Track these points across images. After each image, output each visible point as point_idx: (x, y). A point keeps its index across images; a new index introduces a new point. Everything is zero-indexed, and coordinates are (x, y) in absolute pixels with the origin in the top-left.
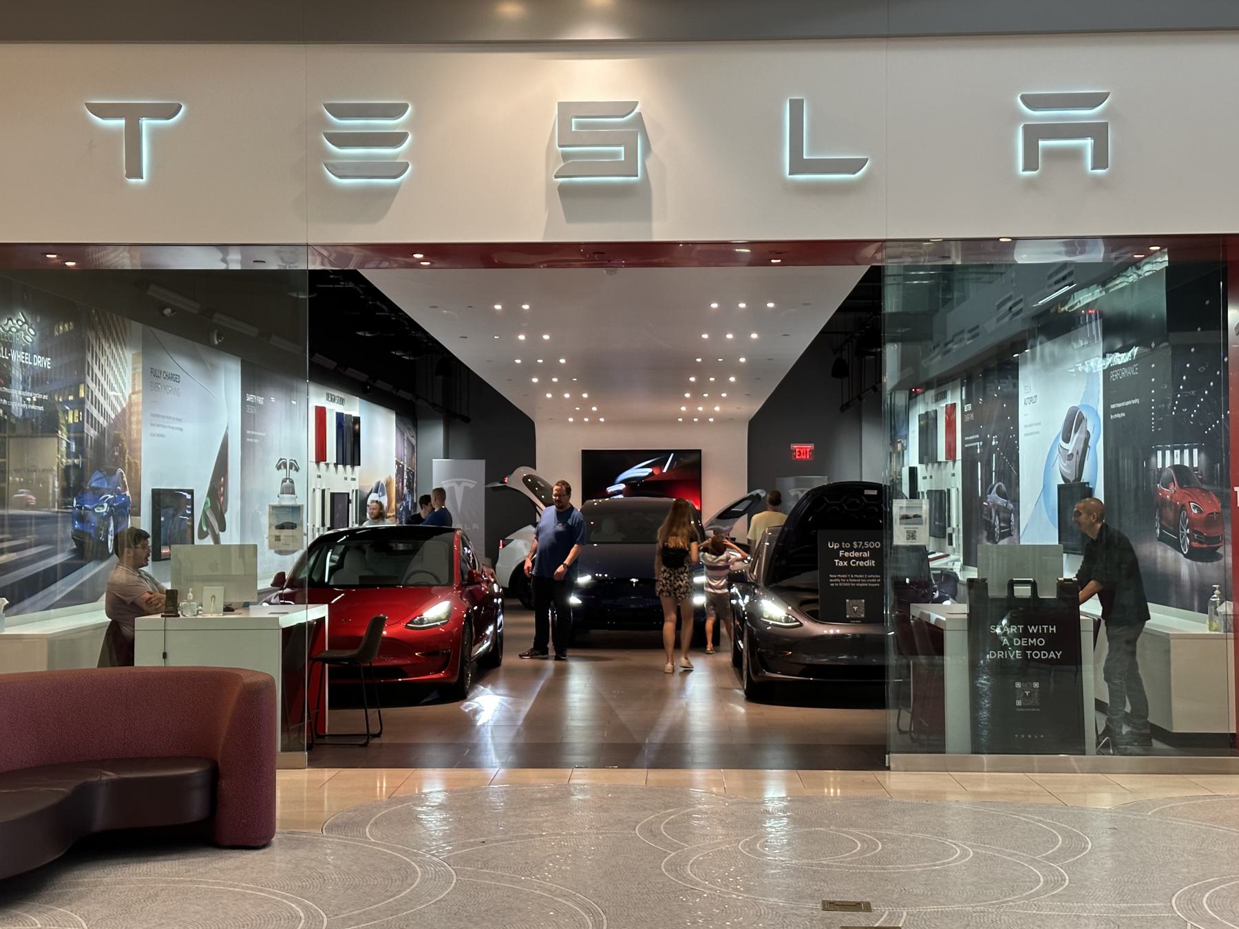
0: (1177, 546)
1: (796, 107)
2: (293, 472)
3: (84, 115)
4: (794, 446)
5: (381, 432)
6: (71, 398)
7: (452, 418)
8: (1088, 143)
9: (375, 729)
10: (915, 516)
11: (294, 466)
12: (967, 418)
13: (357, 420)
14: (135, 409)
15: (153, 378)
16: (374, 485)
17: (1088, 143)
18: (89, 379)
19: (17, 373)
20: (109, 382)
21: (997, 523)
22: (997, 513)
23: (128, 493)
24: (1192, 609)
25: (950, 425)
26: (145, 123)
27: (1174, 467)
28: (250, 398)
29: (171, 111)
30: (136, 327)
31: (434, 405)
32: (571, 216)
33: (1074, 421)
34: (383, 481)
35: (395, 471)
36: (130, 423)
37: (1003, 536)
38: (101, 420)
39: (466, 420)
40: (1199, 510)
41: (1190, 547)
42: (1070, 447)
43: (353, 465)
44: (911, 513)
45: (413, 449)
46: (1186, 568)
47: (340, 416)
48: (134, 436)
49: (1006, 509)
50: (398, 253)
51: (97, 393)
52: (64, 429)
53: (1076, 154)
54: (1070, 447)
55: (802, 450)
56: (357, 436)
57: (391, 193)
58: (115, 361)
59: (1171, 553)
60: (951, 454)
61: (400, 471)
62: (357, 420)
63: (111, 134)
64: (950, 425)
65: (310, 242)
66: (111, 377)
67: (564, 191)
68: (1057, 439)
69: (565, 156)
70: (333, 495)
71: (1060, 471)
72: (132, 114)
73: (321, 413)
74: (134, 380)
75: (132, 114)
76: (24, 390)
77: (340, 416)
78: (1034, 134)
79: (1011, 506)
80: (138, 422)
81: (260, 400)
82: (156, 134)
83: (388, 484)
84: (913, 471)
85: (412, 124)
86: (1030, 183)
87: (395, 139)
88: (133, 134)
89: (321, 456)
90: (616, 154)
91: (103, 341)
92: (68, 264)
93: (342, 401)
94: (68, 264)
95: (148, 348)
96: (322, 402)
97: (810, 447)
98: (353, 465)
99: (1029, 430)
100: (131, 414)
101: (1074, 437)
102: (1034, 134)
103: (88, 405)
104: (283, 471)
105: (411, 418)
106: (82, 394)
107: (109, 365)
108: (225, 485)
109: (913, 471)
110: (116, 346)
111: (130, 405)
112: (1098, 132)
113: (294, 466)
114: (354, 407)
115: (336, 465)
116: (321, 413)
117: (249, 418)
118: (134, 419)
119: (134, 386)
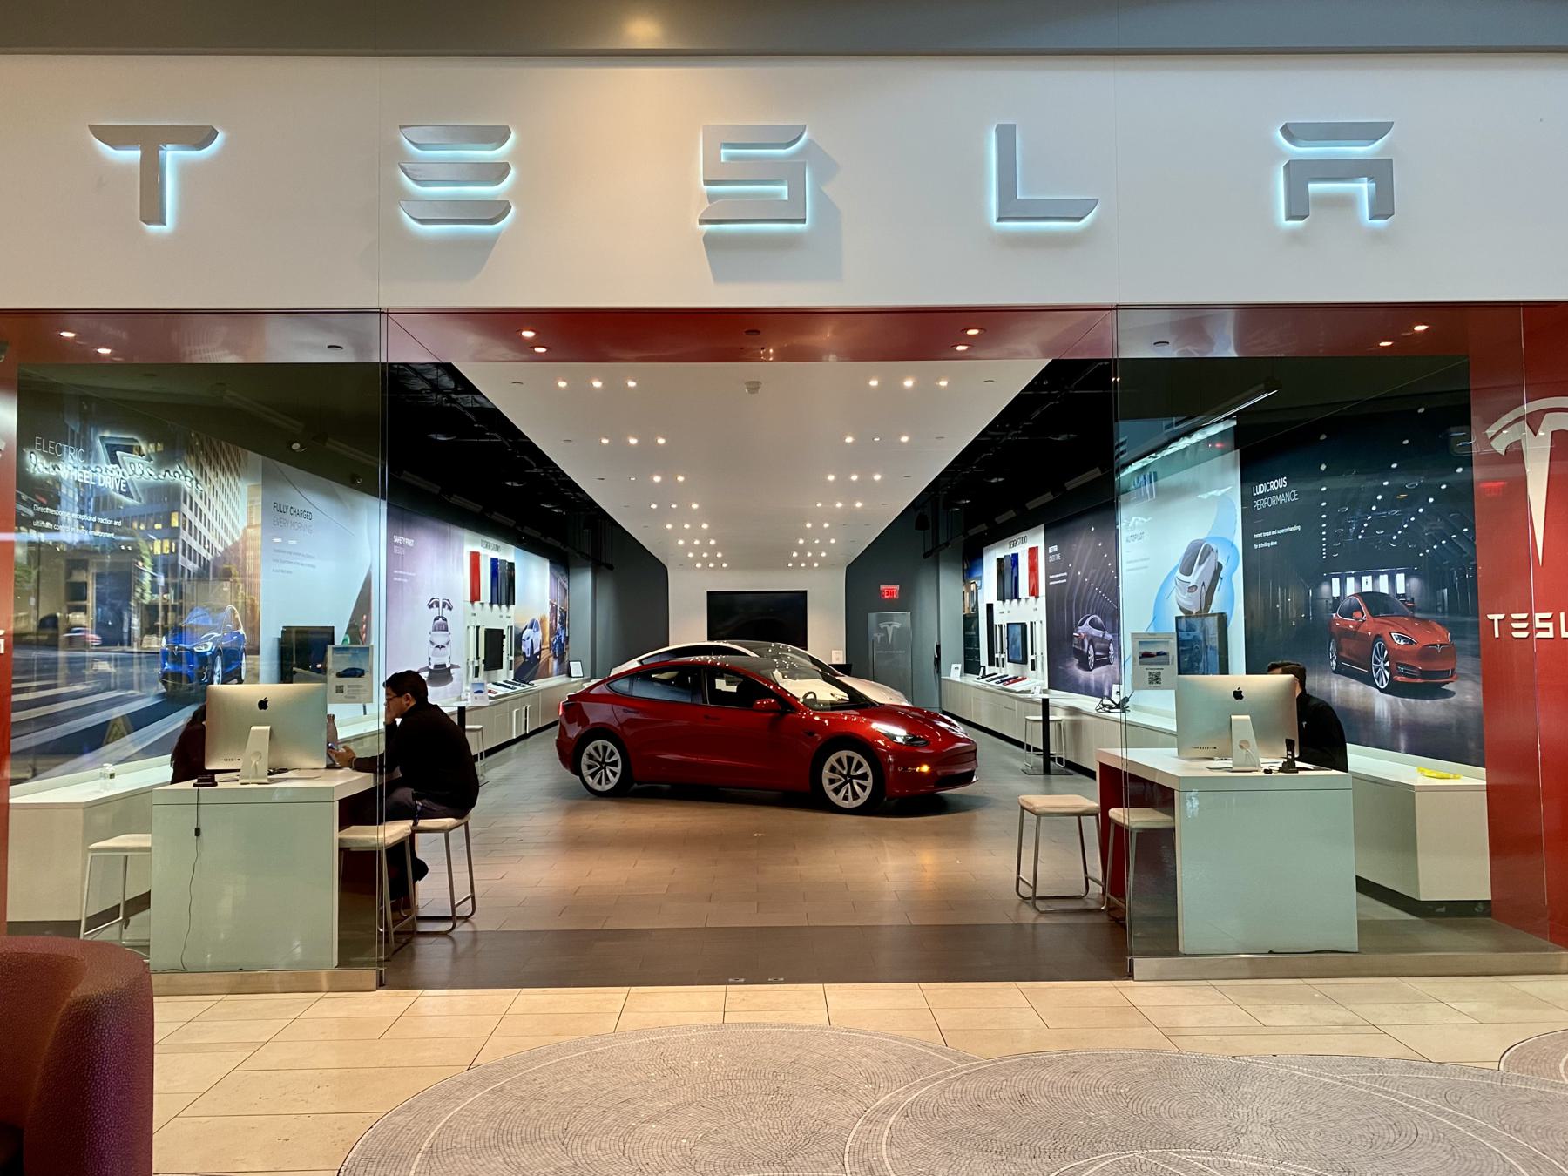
0: (1369, 681)
1: (1006, 135)
2: (446, 610)
3: (96, 155)
4: (882, 587)
5: (536, 580)
6: (158, 526)
7: (599, 566)
8: (1363, 189)
9: (465, 909)
10: (1159, 654)
11: (447, 605)
12: (1052, 559)
13: (512, 565)
14: (250, 543)
15: (276, 514)
16: (528, 622)
17: (1363, 189)
18: (185, 509)
19: (69, 494)
20: (218, 518)
21: (1091, 651)
22: (1091, 642)
23: (242, 631)
24: (1396, 749)
25: (1033, 568)
26: (172, 155)
27: (1361, 595)
28: (397, 539)
29: (203, 137)
30: (255, 459)
31: (581, 553)
32: (720, 275)
33: (1195, 555)
34: (538, 619)
35: (548, 608)
36: (245, 558)
37: (1097, 664)
38: (204, 553)
39: (610, 567)
40: (1406, 640)
41: (1391, 681)
42: (1192, 579)
43: (508, 605)
44: (1153, 650)
45: (566, 591)
46: (1382, 704)
47: (494, 562)
48: (250, 570)
49: (1102, 639)
50: (502, 323)
51: (196, 522)
52: (148, 561)
53: (1347, 202)
54: (1192, 579)
55: (891, 590)
56: (512, 580)
57: (487, 243)
58: (227, 496)
59: (1356, 689)
60: (1034, 592)
61: (554, 609)
62: (512, 565)
63: (126, 168)
64: (1033, 568)
65: (384, 305)
66: (217, 507)
67: (711, 242)
68: (1174, 571)
69: (712, 197)
70: (488, 631)
71: (1178, 601)
72: (150, 140)
73: (475, 557)
74: (250, 513)
75: (150, 140)
76: (82, 512)
77: (494, 562)
78: (1299, 173)
79: (1109, 636)
80: (255, 558)
81: (409, 542)
82: (188, 172)
83: (542, 621)
84: (990, 607)
85: (517, 153)
86: (1294, 236)
87: (497, 172)
88: (152, 170)
89: (475, 597)
90: (777, 194)
91: (207, 469)
92: (64, 334)
93: (497, 549)
94: (64, 334)
95: (269, 479)
96: (477, 548)
97: (897, 588)
98: (508, 605)
99: (1132, 566)
100: (245, 549)
101: (1198, 571)
102: (1299, 173)
103: (184, 535)
104: (435, 609)
105: (562, 562)
106: (175, 523)
107: (215, 493)
108: (368, 622)
109: (990, 607)
110: (224, 473)
111: (245, 538)
112: (1379, 171)
113: (447, 605)
114: (509, 553)
115: (491, 604)
116: (475, 557)
117: (394, 558)
118: (250, 553)
119: (250, 519)
